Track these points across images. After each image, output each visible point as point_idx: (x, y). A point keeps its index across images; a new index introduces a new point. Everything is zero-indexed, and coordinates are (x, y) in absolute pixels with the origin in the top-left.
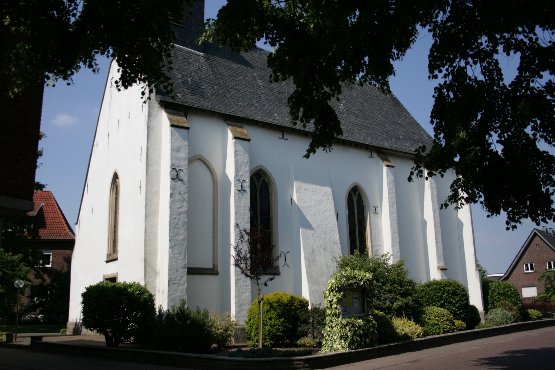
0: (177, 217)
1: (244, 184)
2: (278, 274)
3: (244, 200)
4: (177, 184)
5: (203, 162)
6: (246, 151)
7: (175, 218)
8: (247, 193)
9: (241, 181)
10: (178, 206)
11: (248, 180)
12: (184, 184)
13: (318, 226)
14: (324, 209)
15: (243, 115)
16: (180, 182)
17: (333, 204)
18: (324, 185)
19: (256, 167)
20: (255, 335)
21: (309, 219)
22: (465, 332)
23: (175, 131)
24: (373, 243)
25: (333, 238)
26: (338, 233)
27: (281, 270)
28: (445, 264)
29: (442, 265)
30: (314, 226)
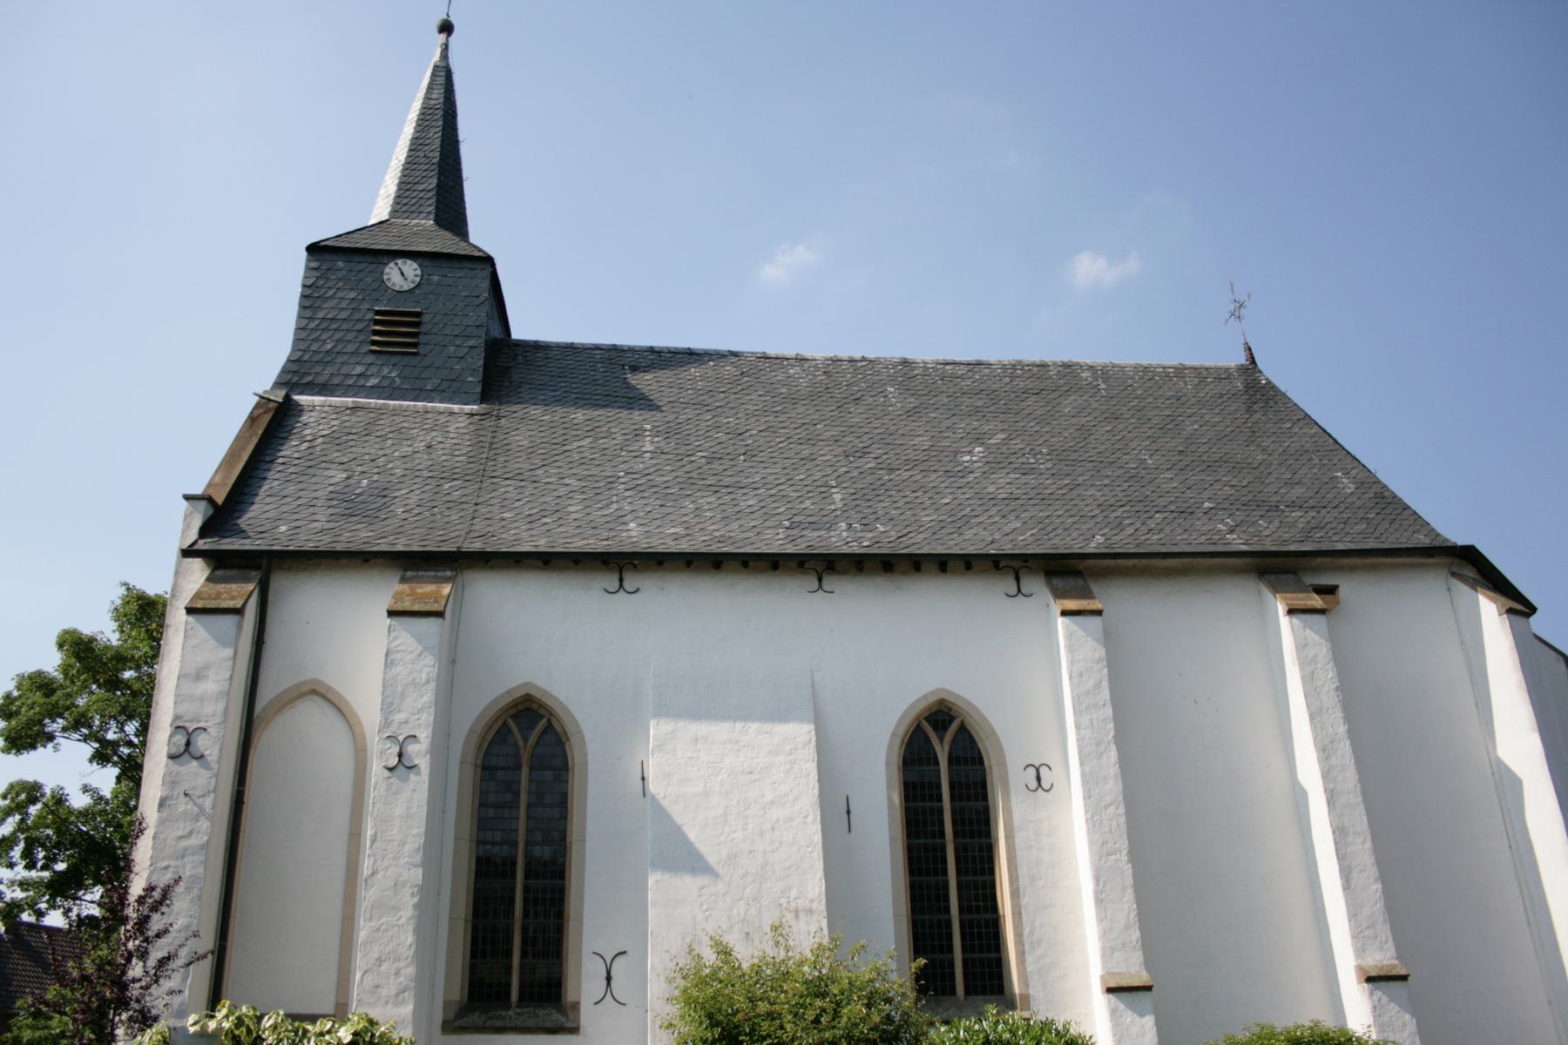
0: (173, 863)
1: (412, 748)
2: (575, 1030)
4: (184, 769)
5: (324, 697)
7: (166, 868)
8: (419, 773)
9: (401, 738)
10: (180, 833)
11: (424, 735)
12: (207, 767)
13: (732, 858)
14: (769, 797)
15: (542, 545)
16: (194, 763)
18: (780, 715)
24: (1024, 901)
25: (794, 893)
26: (820, 874)
28: (1148, 964)
29: (1384, 958)
30: (712, 859)
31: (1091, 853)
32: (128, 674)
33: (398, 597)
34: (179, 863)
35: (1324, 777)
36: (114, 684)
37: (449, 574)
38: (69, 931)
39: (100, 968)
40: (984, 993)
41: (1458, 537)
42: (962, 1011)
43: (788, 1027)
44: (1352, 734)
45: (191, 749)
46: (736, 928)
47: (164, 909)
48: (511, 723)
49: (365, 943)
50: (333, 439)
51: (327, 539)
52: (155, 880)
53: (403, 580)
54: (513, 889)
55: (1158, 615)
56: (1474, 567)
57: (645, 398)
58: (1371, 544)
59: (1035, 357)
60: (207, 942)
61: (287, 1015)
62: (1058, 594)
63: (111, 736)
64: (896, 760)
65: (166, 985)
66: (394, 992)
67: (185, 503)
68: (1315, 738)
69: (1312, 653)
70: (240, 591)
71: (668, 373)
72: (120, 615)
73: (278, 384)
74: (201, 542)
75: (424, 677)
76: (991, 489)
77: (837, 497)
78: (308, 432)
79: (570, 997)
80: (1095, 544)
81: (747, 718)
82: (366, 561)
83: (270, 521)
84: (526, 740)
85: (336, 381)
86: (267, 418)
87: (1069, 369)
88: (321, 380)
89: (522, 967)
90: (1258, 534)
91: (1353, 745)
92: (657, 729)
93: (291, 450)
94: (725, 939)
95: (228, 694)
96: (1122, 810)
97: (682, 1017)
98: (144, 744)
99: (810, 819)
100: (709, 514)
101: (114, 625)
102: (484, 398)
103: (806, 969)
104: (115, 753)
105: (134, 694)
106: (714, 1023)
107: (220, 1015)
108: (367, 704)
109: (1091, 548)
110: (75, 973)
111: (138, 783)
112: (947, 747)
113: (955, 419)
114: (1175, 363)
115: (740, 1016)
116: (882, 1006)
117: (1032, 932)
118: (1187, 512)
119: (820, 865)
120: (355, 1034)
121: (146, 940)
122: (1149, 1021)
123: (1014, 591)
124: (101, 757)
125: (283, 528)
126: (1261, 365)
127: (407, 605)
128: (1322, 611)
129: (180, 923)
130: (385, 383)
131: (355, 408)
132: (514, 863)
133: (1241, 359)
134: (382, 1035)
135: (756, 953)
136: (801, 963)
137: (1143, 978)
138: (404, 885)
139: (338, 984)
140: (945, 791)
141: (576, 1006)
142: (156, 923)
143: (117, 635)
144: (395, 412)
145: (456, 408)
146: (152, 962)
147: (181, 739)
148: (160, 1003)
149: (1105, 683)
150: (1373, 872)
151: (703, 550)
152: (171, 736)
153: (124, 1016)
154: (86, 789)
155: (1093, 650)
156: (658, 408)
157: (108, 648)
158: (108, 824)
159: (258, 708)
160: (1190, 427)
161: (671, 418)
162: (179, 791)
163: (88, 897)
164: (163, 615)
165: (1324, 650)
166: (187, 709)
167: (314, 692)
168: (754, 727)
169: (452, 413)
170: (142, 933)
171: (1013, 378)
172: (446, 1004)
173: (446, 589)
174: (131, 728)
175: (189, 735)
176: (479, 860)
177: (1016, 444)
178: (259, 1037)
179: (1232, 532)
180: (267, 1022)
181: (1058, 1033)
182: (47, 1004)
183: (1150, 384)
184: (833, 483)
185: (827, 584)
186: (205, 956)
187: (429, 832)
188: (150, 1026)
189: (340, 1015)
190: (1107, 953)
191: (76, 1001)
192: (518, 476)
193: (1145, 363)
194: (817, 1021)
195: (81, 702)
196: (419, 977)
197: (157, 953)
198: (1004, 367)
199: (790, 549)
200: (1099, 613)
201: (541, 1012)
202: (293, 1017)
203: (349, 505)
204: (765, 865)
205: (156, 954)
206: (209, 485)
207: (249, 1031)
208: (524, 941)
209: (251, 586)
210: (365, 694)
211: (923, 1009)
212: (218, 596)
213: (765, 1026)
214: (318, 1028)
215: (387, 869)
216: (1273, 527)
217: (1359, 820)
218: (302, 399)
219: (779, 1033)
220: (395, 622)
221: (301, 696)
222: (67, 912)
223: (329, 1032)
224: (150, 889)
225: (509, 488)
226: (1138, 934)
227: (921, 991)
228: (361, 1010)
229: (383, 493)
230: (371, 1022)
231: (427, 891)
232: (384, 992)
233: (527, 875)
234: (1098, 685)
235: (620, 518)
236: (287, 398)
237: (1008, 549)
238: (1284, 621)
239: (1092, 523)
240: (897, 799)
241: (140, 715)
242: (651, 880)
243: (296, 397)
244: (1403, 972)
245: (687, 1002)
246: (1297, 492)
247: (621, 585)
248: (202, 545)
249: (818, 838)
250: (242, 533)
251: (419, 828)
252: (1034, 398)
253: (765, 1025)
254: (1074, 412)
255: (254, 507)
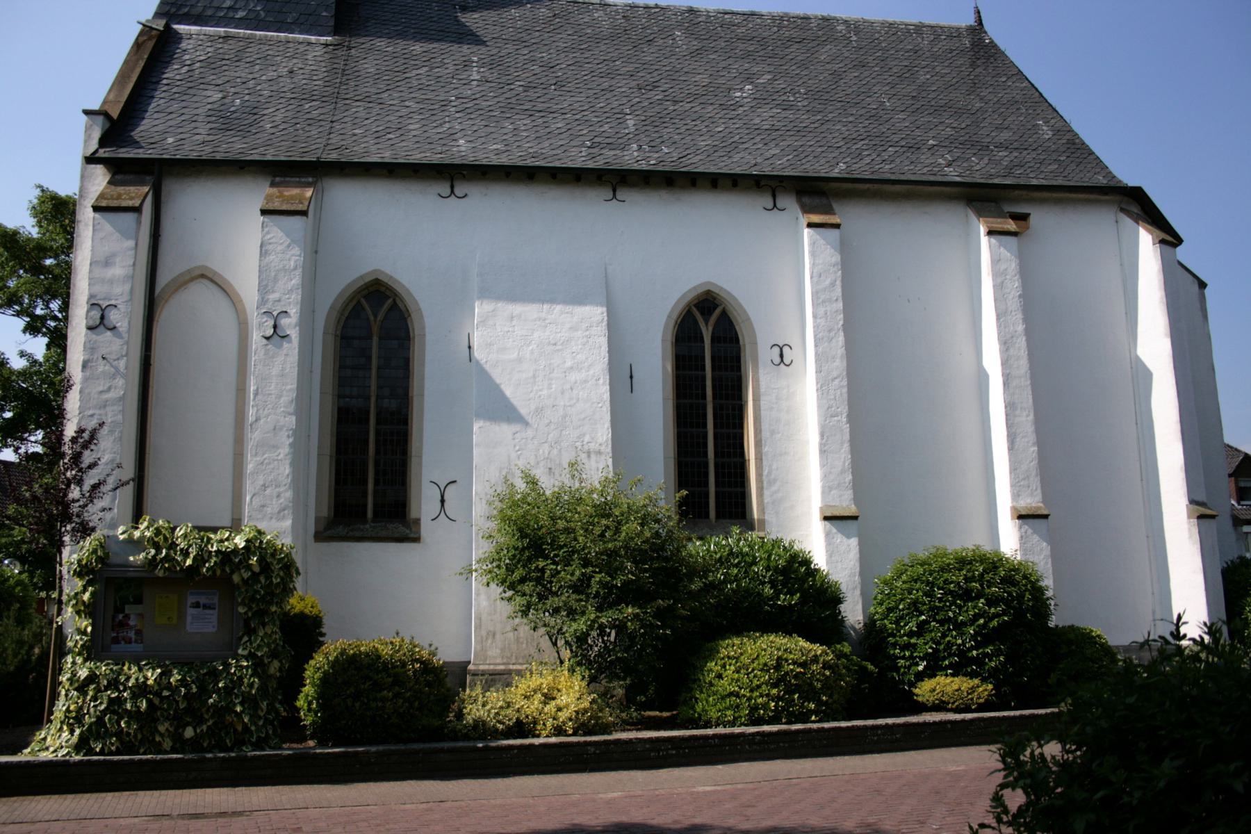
0: (97, 412)
1: (284, 321)
2: (417, 539)
3: (280, 359)
4: (100, 338)
5: (212, 281)
7: (92, 416)
8: (290, 342)
9: (275, 313)
10: (101, 388)
11: (294, 311)
12: (119, 336)
13: (539, 411)
14: (569, 364)
15: (387, 156)
16: (109, 333)
17: (605, 348)
18: (578, 299)
19: (361, 277)
22: (116, 758)
23: (103, 221)
24: (765, 449)
25: (587, 439)
26: (608, 424)
27: (426, 528)
28: (857, 499)
29: (1032, 501)
30: (523, 411)
31: (819, 415)
32: (48, 262)
33: (269, 198)
34: (102, 412)
35: (1002, 364)
36: (38, 269)
37: (310, 180)
38: (19, 464)
39: (47, 491)
40: (730, 517)
41: (1129, 178)
42: (713, 530)
43: (581, 539)
44: (1028, 332)
45: (106, 322)
46: (542, 464)
47: (93, 447)
48: (370, 514)
49: (252, 473)
50: (208, 63)
51: (208, 149)
52: (84, 424)
53: (273, 185)
54: (368, 432)
55: (886, 231)
56: (1139, 205)
57: (473, 34)
58: (1060, 181)
59: (799, 11)
60: (129, 472)
61: (194, 527)
62: (806, 210)
63: (39, 312)
64: (670, 338)
65: (100, 504)
66: (276, 510)
67: (84, 118)
68: (999, 334)
69: (1003, 267)
70: (136, 193)
71: (493, 13)
72: (37, 212)
73: (158, 15)
74: (101, 151)
75: (292, 263)
76: (757, 121)
77: (631, 123)
78: (187, 57)
79: (413, 514)
80: (838, 170)
81: (553, 301)
82: (242, 168)
83: (159, 133)
84: (376, 317)
85: (209, 12)
86: (151, 44)
87: (827, 22)
88: (196, 11)
89: (375, 492)
90: (970, 168)
91: (1028, 341)
92: (480, 308)
93: (173, 73)
94: (533, 472)
95: (133, 277)
96: (845, 383)
97: (499, 531)
98: (66, 318)
99: (601, 381)
100: (525, 134)
101: (33, 221)
102: (336, 32)
103: (595, 496)
104: (44, 325)
105: (56, 278)
106: (523, 535)
107: (142, 527)
108: (247, 286)
109: (835, 173)
110: (27, 494)
111: (64, 350)
112: (710, 328)
113: (730, 61)
114: (915, 21)
115: (544, 530)
116: (653, 525)
117: (770, 473)
118: (915, 148)
119: (608, 417)
120: (247, 541)
121: (80, 470)
122: (854, 542)
123: (770, 205)
124: (33, 328)
125: (170, 140)
126: (987, 26)
127: (277, 205)
128: (1015, 234)
129: (106, 458)
130: (252, 16)
131: (226, 38)
132: (368, 412)
133: (970, 21)
134: (269, 542)
135: (557, 483)
136: (592, 492)
137: (852, 510)
138: (281, 429)
139: (233, 504)
140: (708, 362)
141: (417, 522)
142: (87, 458)
143: (37, 229)
144: (261, 41)
145: (313, 38)
146: (86, 487)
147: (96, 314)
148: (95, 518)
149: (839, 283)
150: (1032, 438)
151: (520, 164)
152: (88, 312)
153: (69, 527)
154: (22, 354)
155: (831, 256)
156: (484, 43)
157: (30, 240)
158: (43, 382)
159: (158, 289)
160: (923, 77)
161: (494, 51)
162: (97, 355)
163: (32, 438)
164: (74, 213)
165: (1014, 265)
166: (100, 289)
167: (203, 276)
168: (558, 308)
169: (309, 43)
170: (77, 466)
171: (780, 27)
172: (317, 520)
173: (309, 193)
174: (55, 305)
175: (103, 310)
176: (340, 409)
177: (781, 84)
178: (173, 543)
179: (949, 165)
180: (179, 532)
181: (785, 548)
182: (8, 518)
183: (894, 38)
184: (628, 111)
185: (620, 195)
186: (127, 483)
187: (300, 388)
188: (89, 535)
189: (236, 527)
190: (826, 490)
191: (30, 516)
192: (367, 98)
193: (891, 20)
194: (602, 535)
195: (12, 284)
196: (295, 500)
197: (90, 480)
198: (773, 18)
199: (591, 165)
200: (837, 226)
201: (390, 526)
202: (200, 529)
203: (225, 120)
204: (564, 417)
205: (89, 481)
206: (105, 102)
207: (166, 539)
208: (377, 473)
209: (146, 189)
210: (246, 279)
211: (683, 528)
212: (119, 197)
213: (562, 538)
214: (218, 536)
215: (267, 416)
216: (982, 164)
217: (1027, 399)
218: (181, 28)
219: (574, 543)
220: (267, 219)
221: (192, 279)
222: (16, 450)
223: (227, 539)
224: (80, 431)
225: (359, 109)
226: (850, 477)
227: (683, 515)
228: (251, 524)
229: (254, 110)
230: (260, 532)
231: (299, 434)
232: (269, 510)
233: (378, 422)
234: (833, 284)
235: (452, 135)
236: (167, 26)
237: (767, 171)
238: (984, 240)
239: (836, 153)
240: (669, 368)
241: (61, 295)
242: (476, 428)
243: (175, 26)
244: (1046, 512)
245: (503, 520)
246: (1005, 135)
247: (452, 192)
248: (102, 153)
249: (607, 396)
250: (135, 144)
251: (291, 385)
252: (796, 46)
253: (563, 537)
254: (828, 59)
255: (145, 122)
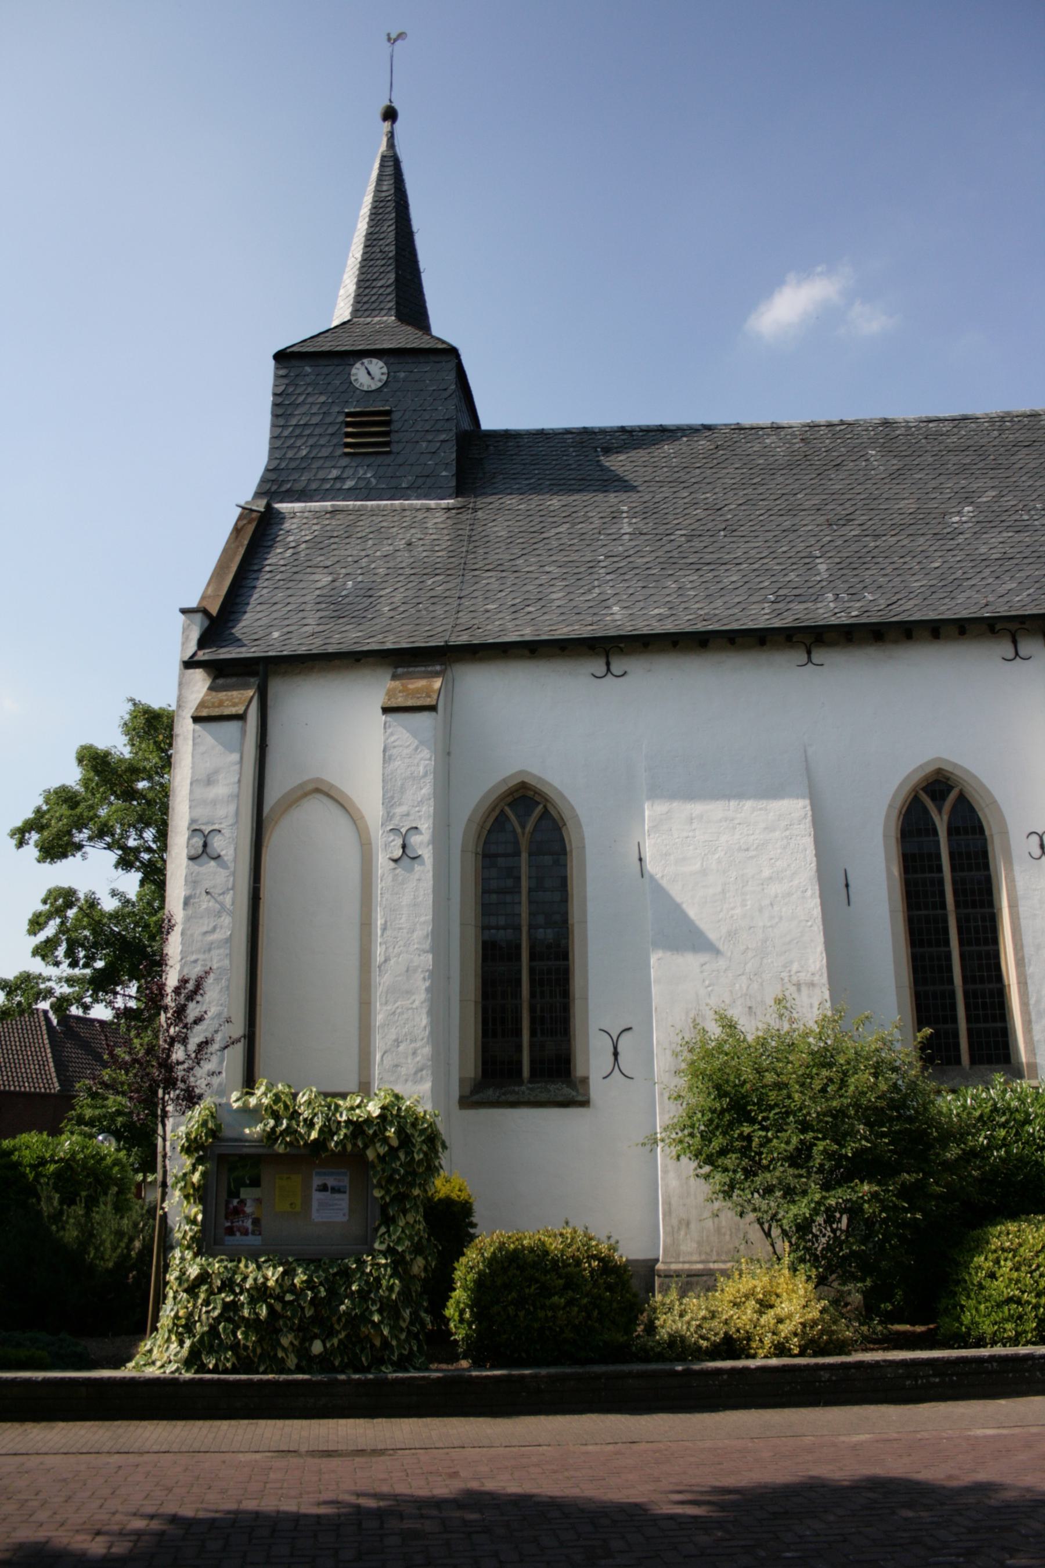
0: (201, 956)
1: (414, 840)
2: (585, 1103)
4: (203, 869)
6: (422, 743)
7: (196, 961)
8: (423, 864)
10: (205, 929)
12: (224, 866)
15: (528, 634)
16: (213, 863)
18: (774, 792)
19: (504, 780)
20: (985, 1297)
21: (692, 913)
25: (795, 967)
26: (820, 948)
27: (597, 1088)
30: (712, 936)
